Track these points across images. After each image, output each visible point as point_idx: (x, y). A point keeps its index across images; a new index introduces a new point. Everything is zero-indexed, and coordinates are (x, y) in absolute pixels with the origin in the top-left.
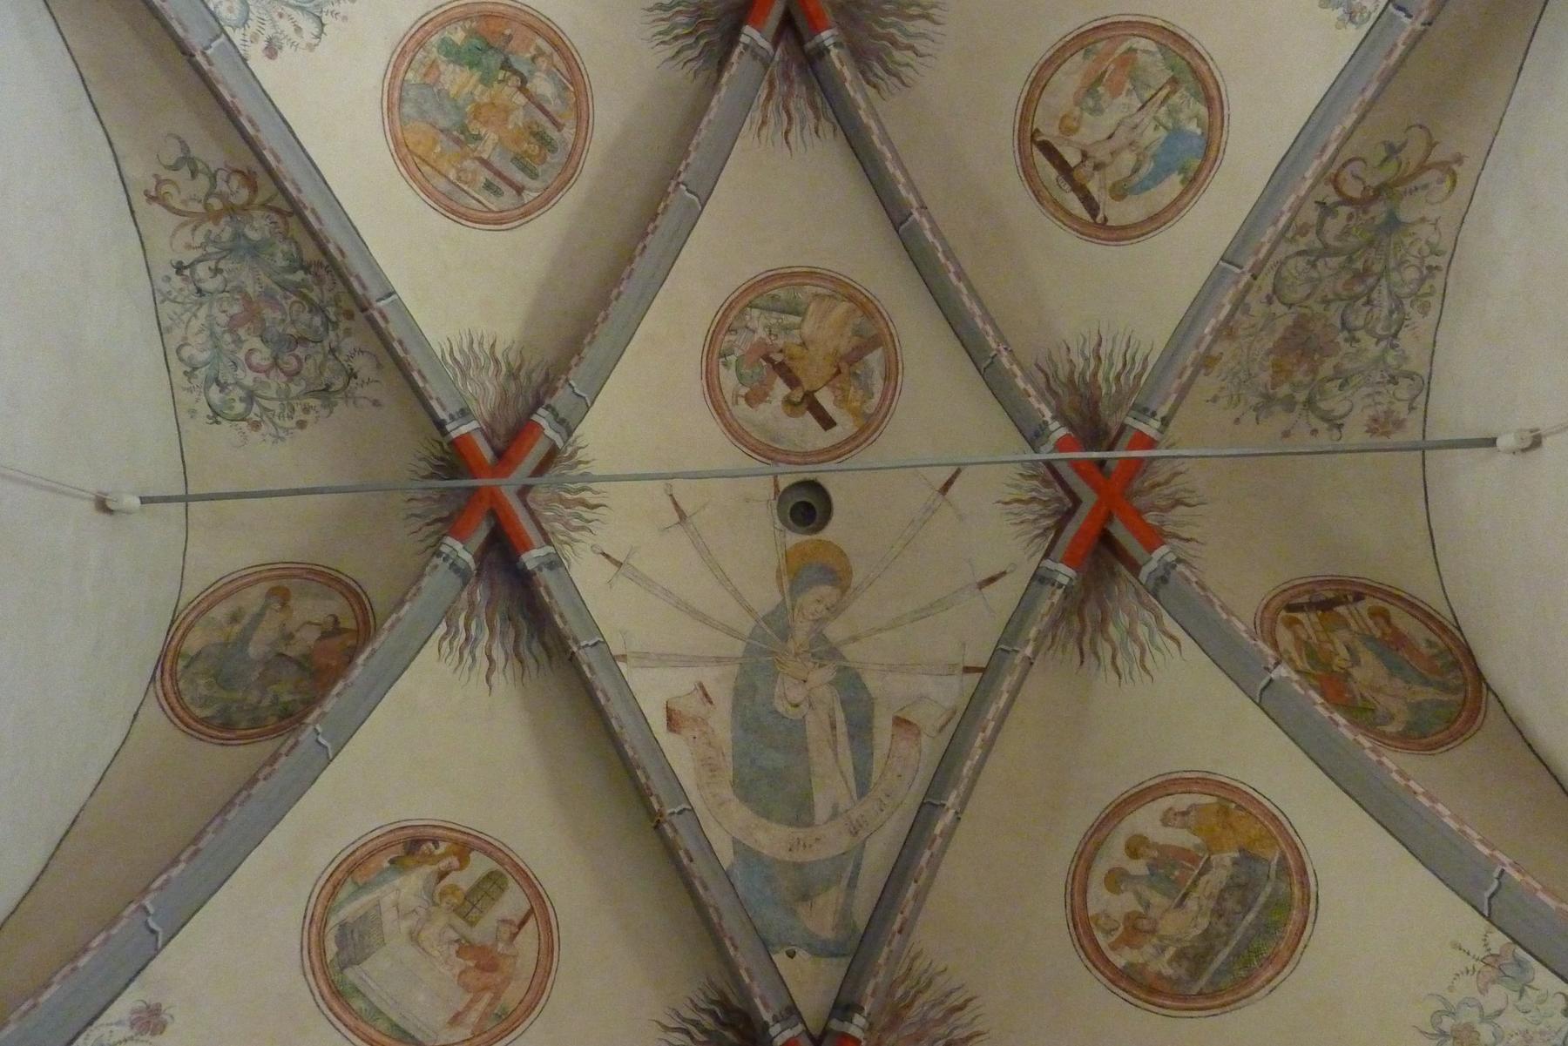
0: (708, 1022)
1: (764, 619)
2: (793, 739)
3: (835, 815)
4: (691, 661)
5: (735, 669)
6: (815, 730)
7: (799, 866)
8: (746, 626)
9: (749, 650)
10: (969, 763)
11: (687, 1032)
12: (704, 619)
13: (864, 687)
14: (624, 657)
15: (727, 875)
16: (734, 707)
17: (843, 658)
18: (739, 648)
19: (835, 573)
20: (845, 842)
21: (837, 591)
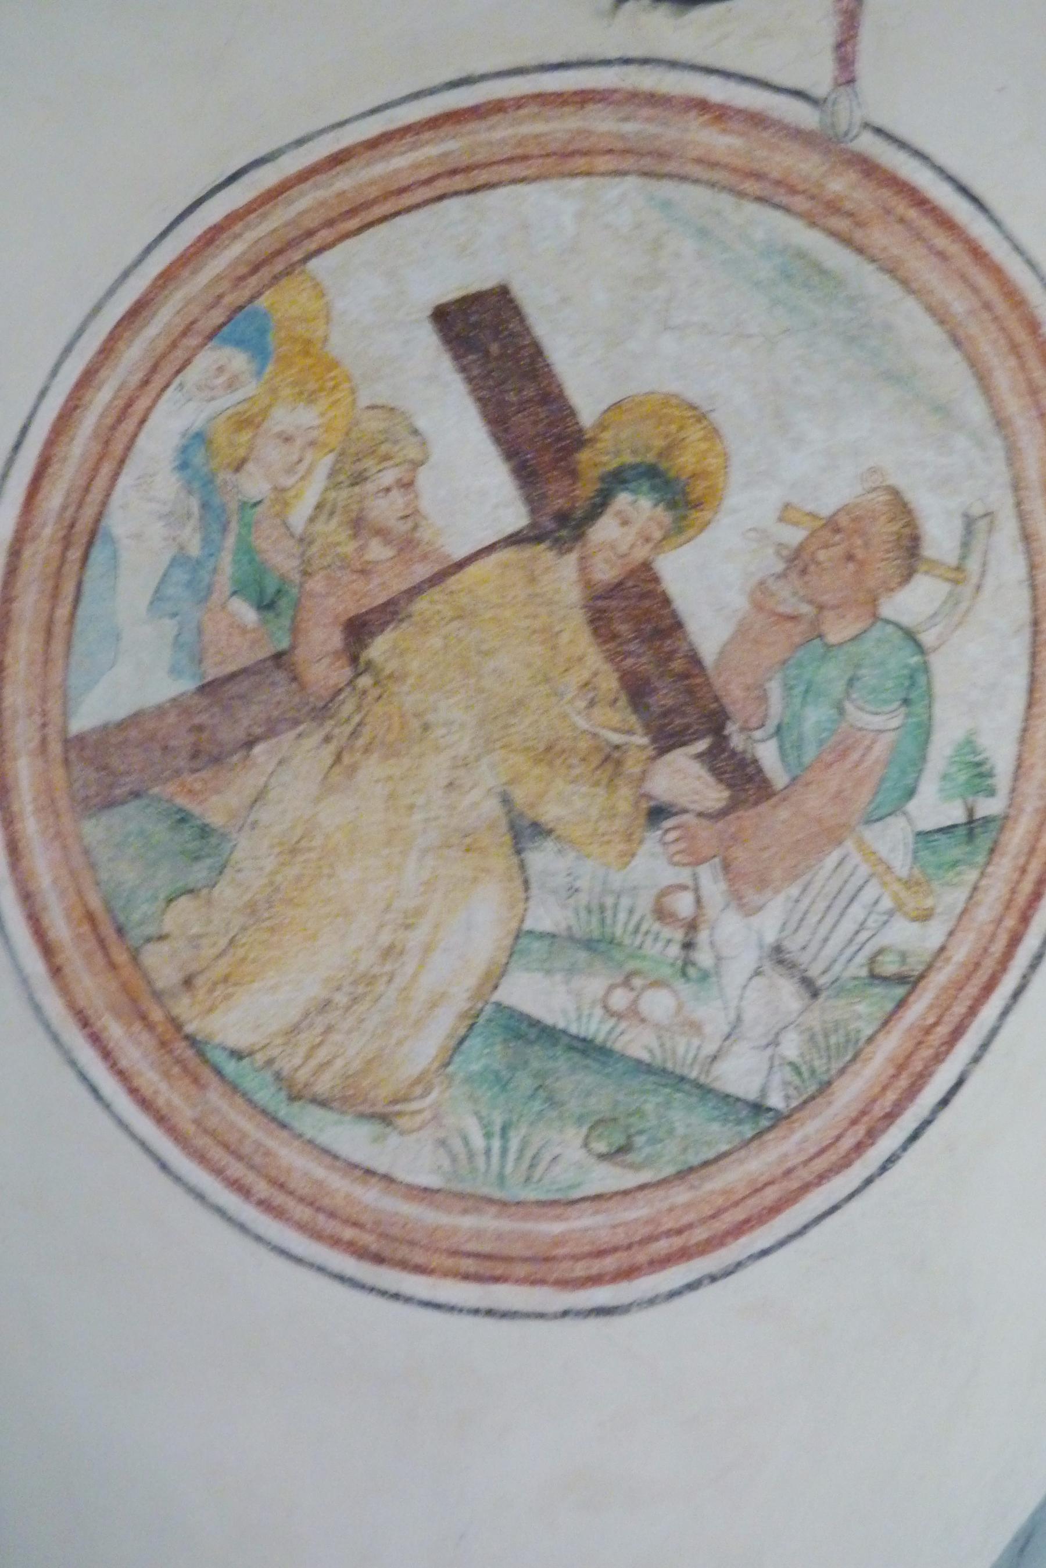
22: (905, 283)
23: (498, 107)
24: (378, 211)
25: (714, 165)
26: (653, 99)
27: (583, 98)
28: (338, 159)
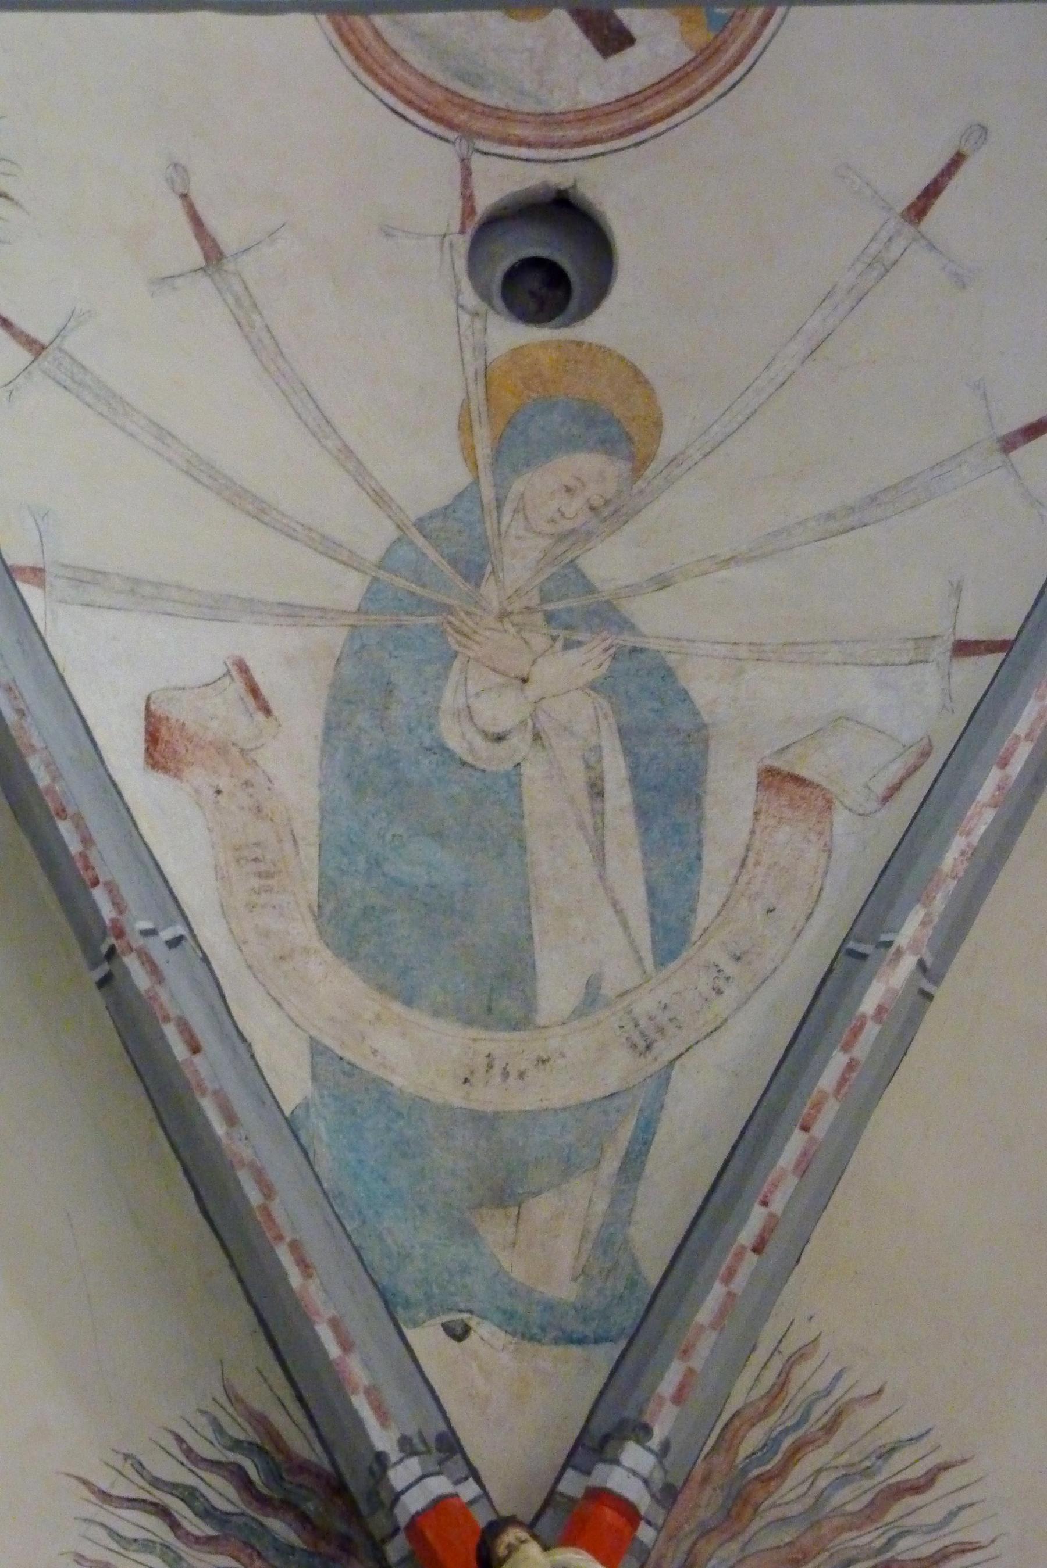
0: (221, 1493)
1: (420, 524)
2: (489, 813)
3: (592, 998)
4: (216, 608)
5: (336, 637)
6: (546, 796)
7: (486, 1122)
8: (374, 536)
9: (373, 593)
10: (959, 843)
11: (164, 1513)
12: (260, 511)
13: (684, 696)
14: (37, 574)
15: (292, 1125)
16: (329, 729)
17: (627, 625)
18: (351, 588)
19: (619, 425)
20: (618, 1069)
21: (623, 467)
22: (424, 77)
23: (621, 135)
24: (667, 83)
25: (521, 121)
26: (552, 146)
27: (585, 142)
28: (689, 102)
